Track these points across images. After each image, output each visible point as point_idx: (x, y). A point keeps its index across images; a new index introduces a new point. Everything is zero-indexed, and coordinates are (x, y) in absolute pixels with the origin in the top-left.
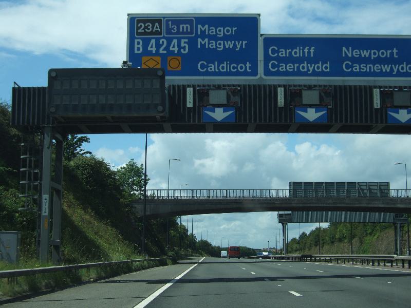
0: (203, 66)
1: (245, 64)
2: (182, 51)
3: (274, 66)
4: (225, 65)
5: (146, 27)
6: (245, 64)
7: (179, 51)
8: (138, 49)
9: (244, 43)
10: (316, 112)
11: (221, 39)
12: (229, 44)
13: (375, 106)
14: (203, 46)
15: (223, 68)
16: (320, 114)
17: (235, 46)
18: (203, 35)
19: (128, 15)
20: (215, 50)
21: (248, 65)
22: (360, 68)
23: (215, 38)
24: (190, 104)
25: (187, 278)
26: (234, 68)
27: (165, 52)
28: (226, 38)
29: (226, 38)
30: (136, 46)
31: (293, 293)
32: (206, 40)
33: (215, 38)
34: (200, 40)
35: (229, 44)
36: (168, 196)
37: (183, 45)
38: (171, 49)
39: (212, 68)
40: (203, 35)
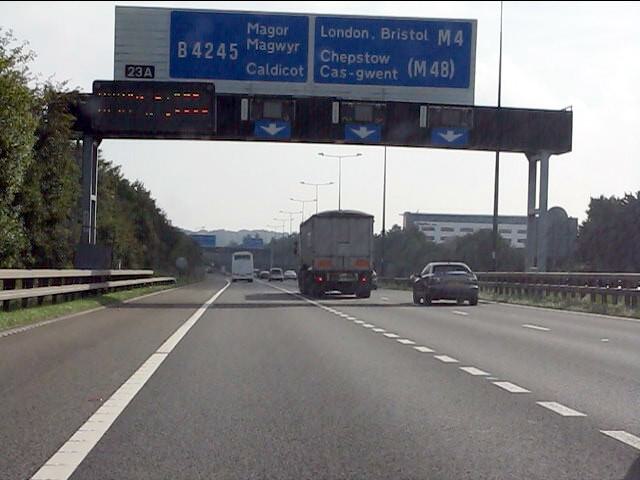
0: (251, 68)
1: (298, 68)
2: (231, 56)
3: (325, 70)
4: (277, 69)
5: (136, 72)
6: (298, 68)
7: (227, 56)
8: (182, 53)
9: (297, 45)
10: (277, 127)
11: (272, 40)
12: (281, 47)
13: (334, 121)
14: (253, 47)
15: (274, 71)
16: (280, 129)
17: (287, 49)
18: (254, 35)
19: (476, 21)
20: (265, 52)
21: (395, 72)
22: (339, 74)
23: (266, 39)
24: (244, 116)
25: (219, 302)
26: (286, 72)
27: (211, 57)
28: (278, 39)
29: (278, 39)
30: (180, 49)
31: (566, 411)
32: (256, 40)
33: (266, 39)
34: (249, 41)
35: (281, 47)
36: (384, 231)
37: (232, 49)
38: (219, 54)
39: (262, 71)
40: (254, 35)
